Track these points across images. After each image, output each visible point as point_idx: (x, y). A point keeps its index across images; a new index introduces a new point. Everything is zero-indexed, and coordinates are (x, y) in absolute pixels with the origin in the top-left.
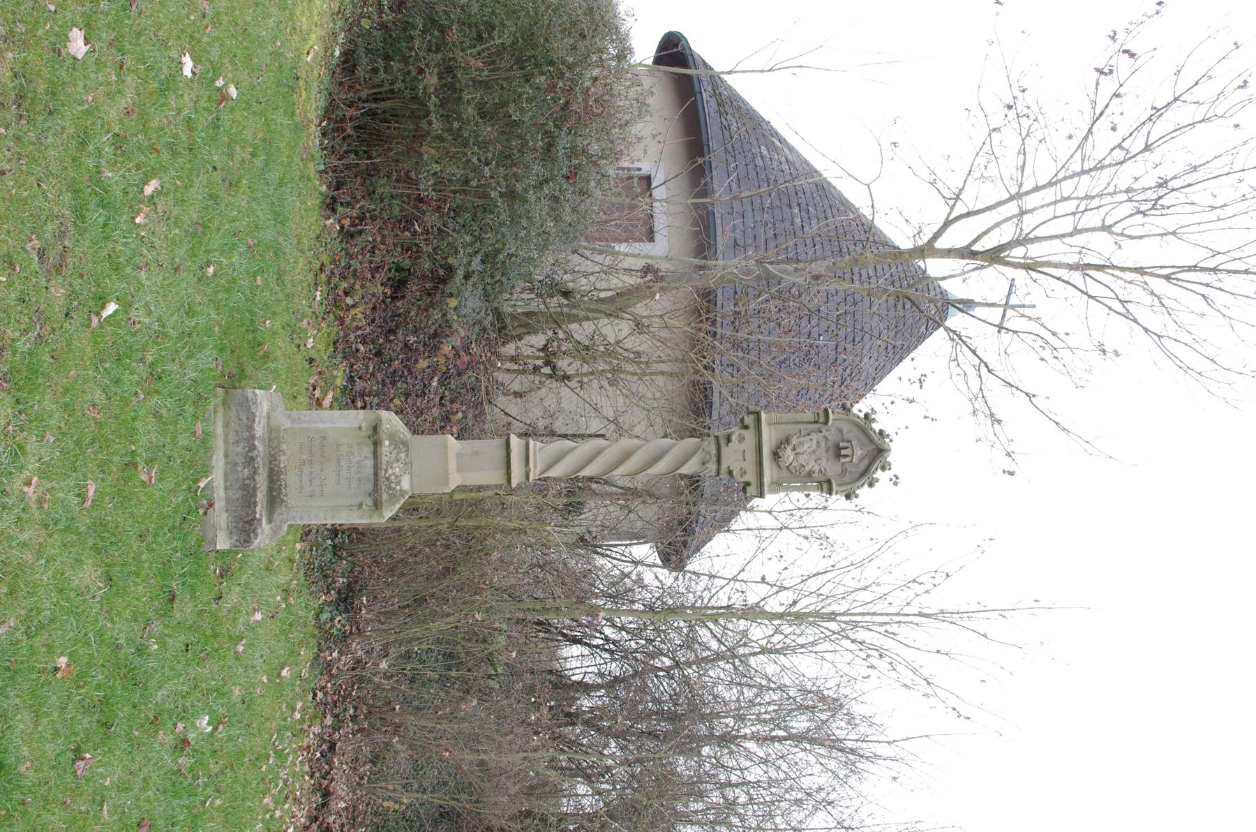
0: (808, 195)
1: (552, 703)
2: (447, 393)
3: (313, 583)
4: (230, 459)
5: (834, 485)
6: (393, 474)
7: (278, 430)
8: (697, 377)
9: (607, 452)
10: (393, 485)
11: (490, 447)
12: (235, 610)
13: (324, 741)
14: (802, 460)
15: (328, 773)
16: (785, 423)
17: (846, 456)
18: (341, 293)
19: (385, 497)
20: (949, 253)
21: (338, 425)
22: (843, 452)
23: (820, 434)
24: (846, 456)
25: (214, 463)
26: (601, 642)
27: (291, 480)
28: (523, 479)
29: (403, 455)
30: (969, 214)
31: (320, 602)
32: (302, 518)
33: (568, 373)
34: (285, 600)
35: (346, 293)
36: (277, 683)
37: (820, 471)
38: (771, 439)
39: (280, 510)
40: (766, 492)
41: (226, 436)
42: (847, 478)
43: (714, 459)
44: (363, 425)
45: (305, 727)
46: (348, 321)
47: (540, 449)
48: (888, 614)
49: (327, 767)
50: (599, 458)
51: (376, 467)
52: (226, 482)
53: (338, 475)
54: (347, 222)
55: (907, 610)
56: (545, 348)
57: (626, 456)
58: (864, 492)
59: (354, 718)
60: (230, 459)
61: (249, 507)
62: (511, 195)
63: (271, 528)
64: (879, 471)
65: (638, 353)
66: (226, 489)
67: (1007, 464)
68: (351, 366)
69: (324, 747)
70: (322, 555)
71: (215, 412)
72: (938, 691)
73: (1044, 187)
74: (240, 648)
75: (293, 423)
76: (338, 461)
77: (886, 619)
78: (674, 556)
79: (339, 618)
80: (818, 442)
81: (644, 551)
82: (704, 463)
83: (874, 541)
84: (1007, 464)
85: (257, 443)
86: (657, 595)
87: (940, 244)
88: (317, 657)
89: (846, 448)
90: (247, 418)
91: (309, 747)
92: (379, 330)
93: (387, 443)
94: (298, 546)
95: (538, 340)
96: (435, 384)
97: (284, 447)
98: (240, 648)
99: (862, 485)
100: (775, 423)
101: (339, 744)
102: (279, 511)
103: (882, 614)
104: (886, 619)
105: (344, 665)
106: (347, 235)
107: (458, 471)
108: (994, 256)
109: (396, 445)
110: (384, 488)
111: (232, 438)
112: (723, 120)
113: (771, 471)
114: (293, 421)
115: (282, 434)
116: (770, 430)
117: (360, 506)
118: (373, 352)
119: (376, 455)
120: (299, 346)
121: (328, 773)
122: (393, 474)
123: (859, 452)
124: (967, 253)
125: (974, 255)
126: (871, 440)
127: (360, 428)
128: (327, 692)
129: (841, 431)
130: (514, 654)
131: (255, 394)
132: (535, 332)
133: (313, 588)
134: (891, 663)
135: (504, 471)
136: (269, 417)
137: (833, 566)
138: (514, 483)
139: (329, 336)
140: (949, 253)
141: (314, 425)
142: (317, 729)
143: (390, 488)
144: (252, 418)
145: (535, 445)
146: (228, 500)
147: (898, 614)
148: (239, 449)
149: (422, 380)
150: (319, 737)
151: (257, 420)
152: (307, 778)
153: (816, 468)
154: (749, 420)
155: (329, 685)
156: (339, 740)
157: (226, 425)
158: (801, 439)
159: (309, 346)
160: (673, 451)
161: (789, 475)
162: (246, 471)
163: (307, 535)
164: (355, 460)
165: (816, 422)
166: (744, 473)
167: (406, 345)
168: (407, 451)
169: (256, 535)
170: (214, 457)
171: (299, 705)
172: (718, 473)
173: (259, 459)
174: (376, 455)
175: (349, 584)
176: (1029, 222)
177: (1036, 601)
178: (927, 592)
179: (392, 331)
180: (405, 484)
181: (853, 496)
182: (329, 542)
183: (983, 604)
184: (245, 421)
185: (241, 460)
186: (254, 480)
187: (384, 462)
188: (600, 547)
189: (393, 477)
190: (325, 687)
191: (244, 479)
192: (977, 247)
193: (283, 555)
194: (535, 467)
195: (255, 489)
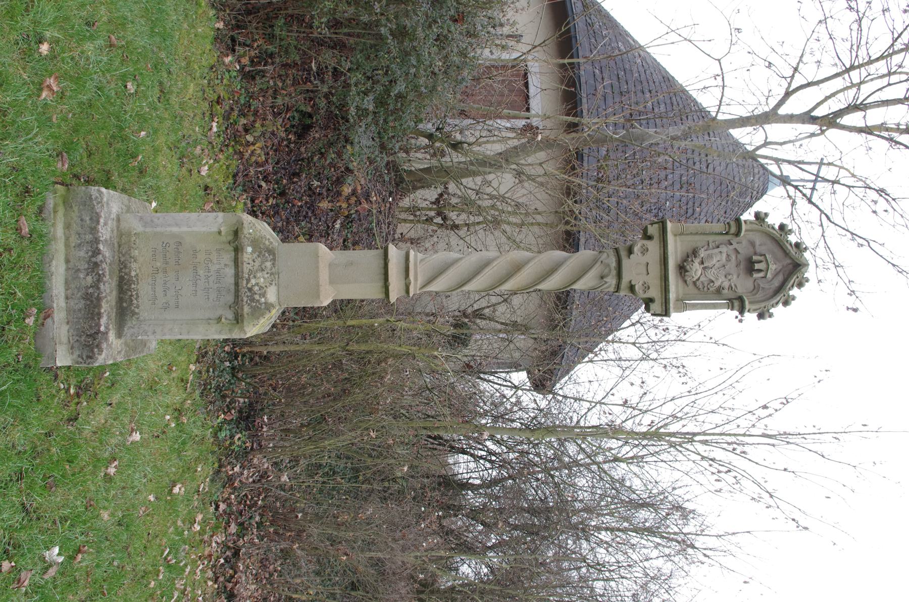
0: (657, 84)
1: (440, 513)
2: (349, 236)
4: (71, 265)
5: (747, 303)
6: (257, 284)
7: (129, 234)
8: (568, 228)
9: (495, 263)
10: (257, 297)
11: (366, 258)
12: (102, 431)
13: (229, 548)
14: (711, 275)
15: (232, 577)
16: (691, 234)
17: (760, 271)
18: (240, 129)
19: (246, 309)
20: (790, 118)
21: (195, 229)
22: (757, 266)
23: (731, 247)
24: (760, 271)
25: (53, 269)
26: (484, 453)
27: (143, 290)
28: (403, 293)
29: (268, 264)
30: (809, 84)
31: (219, 421)
33: (456, 223)
34: (177, 419)
35: (247, 131)
36: (169, 502)
37: (730, 287)
38: (676, 252)
39: (131, 323)
40: (671, 310)
41: (67, 239)
42: (760, 296)
43: (614, 272)
44: (222, 229)
45: (206, 537)
46: (247, 155)
47: (422, 260)
48: (735, 435)
49: (231, 572)
50: (486, 270)
51: (237, 276)
52: (67, 290)
54: (245, 61)
55: (753, 431)
56: (437, 201)
57: (517, 268)
58: (778, 311)
59: (260, 525)
60: (71, 265)
61: (93, 319)
62: (401, 33)
64: (795, 288)
65: (518, 205)
66: (67, 298)
67: (851, 302)
68: (253, 201)
69: (228, 553)
71: (55, 212)
72: (779, 503)
73: (877, 60)
74: (112, 471)
75: (145, 226)
77: (733, 439)
78: (541, 385)
79: (239, 435)
80: (728, 255)
81: (520, 377)
82: (602, 278)
83: (723, 370)
84: (851, 302)
85: (101, 247)
86: (532, 415)
87: (783, 111)
88: (218, 472)
89: (760, 262)
90: (91, 219)
91: (210, 556)
92: (283, 172)
93: (249, 249)
94: (192, 367)
95: (431, 194)
96: (337, 226)
97: (136, 253)
98: (112, 471)
99: (777, 303)
100: (682, 234)
101: (243, 550)
102: (129, 324)
103: (730, 435)
104: (733, 439)
105: (247, 478)
106: (249, 76)
107: (332, 282)
108: (830, 121)
109: (260, 253)
110: (245, 299)
111: (74, 240)
112: (587, 18)
113: (677, 286)
114: (145, 225)
115: (133, 239)
116: (675, 241)
117: (219, 319)
118: (278, 191)
119: (237, 262)
121: (232, 577)
122: (257, 284)
123: (773, 267)
124: (808, 118)
125: (814, 120)
126: (786, 253)
127: (220, 233)
128: (231, 503)
129: (752, 244)
130: (406, 469)
131: (100, 193)
132: (429, 186)
134: (735, 477)
135: (381, 284)
136: (118, 220)
137: (689, 392)
138: (393, 298)
139: (228, 168)
140: (790, 118)
141: (168, 229)
142: (220, 538)
143: (253, 300)
144: (96, 219)
145: (416, 256)
146: (69, 311)
147: (744, 435)
148: (82, 254)
149: (326, 222)
150: (225, 546)
151: (102, 221)
152: (210, 583)
153: (726, 284)
154: (653, 230)
155: (233, 496)
156: (243, 546)
157: (67, 226)
158: (709, 252)
159: (203, 173)
160: (568, 263)
161: (696, 291)
162: (89, 279)
163: (203, 357)
164: (214, 268)
165: (727, 233)
166: (647, 288)
167: (310, 189)
168: (274, 259)
169: (101, 351)
170: (54, 263)
171: (199, 517)
172: (618, 288)
173: (104, 265)
174: (237, 262)
175: (251, 404)
176: (866, 89)
177: (865, 425)
178: (770, 415)
179: (296, 174)
180: (272, 295)
181: (767, 315)
182: (227, 364)
183: (817, 427)
184: (88, 222)
185: (83, 266)
186: (98, 288)
187: (246, 271)
188: (485, 373)
189: (256, 288)
190: (229, 499)
191: (87, 288)
192: (816, 113)
194: (416, 279)
195: (99, 299)
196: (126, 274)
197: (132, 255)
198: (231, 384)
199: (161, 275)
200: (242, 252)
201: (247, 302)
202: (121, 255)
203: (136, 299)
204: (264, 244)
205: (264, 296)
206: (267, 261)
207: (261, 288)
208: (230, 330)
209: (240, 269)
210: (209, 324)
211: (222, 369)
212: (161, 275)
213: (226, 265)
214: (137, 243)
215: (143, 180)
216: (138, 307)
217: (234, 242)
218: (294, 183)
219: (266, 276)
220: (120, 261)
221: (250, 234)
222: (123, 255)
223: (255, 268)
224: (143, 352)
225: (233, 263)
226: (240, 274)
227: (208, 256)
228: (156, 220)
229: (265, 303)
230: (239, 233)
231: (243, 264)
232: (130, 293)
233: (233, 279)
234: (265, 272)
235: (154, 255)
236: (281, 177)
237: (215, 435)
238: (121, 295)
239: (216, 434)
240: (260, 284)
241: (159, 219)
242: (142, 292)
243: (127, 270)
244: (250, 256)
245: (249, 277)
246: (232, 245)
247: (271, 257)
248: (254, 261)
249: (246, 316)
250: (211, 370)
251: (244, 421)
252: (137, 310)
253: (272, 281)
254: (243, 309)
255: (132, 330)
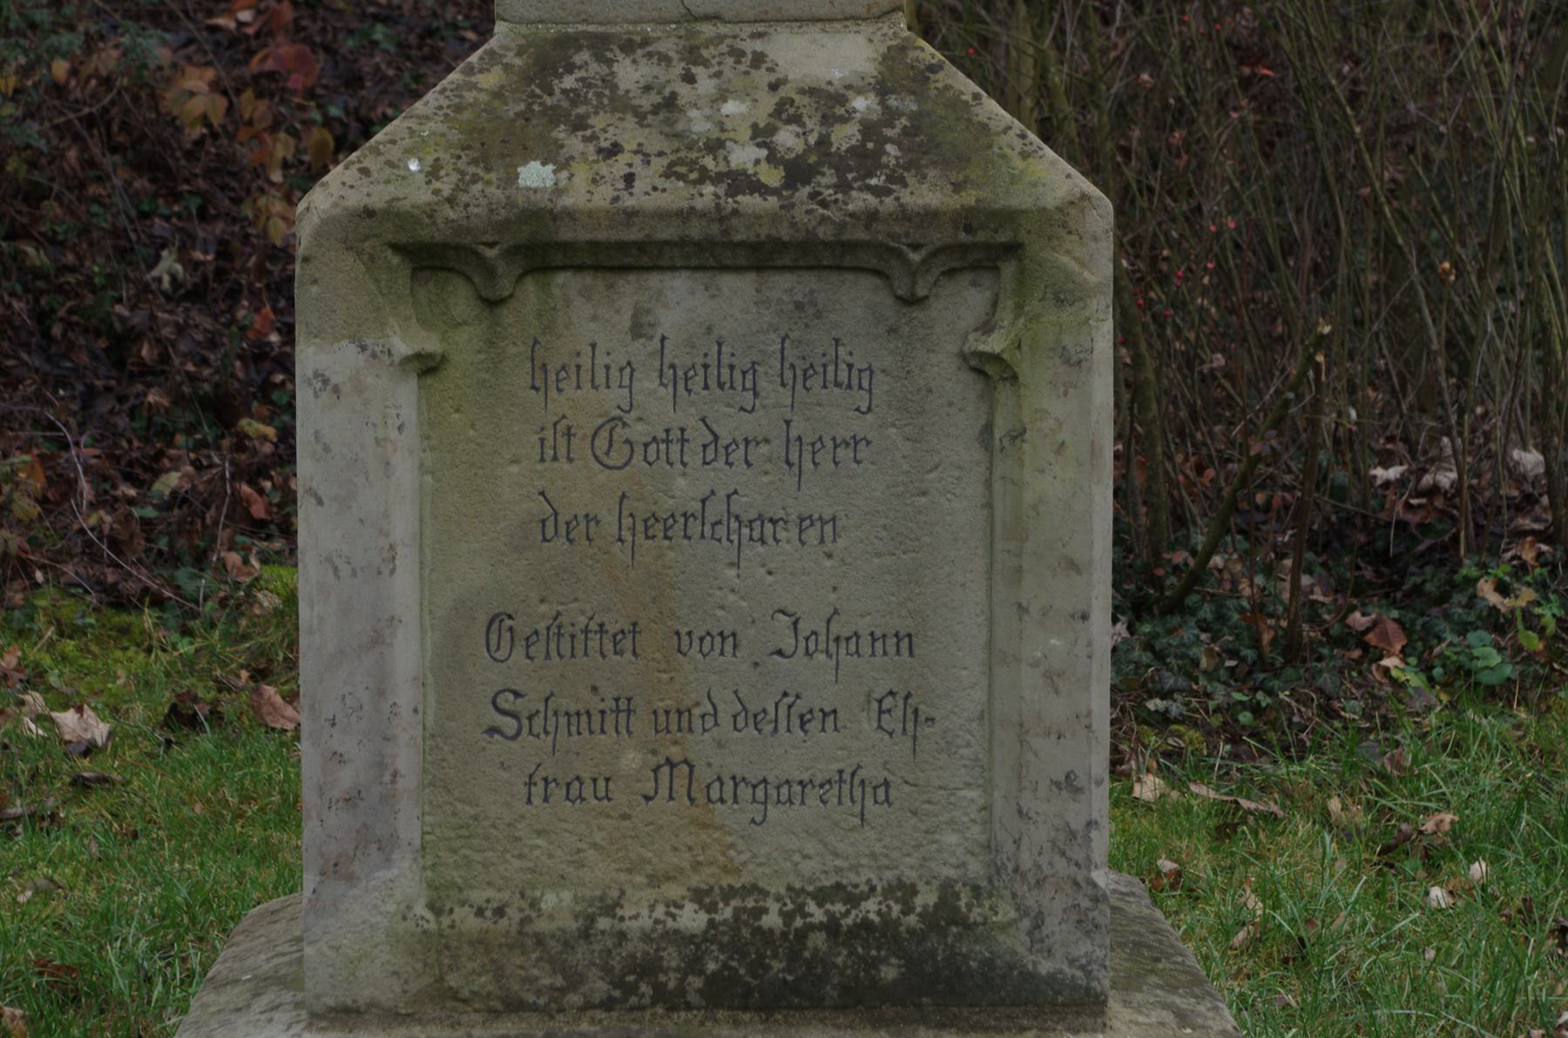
3: (1330, 713)
6: (762, 135)
10: (845, 136)
19: (925, 194)
21: (403, 526)
29: (630, 74)
31: (1415, 680)
32: (1070, 784)
34: (1433, 861)
44: (402, 348)
53: (765, 524)
63: (1129, 983)
70: (1190, 668)
75: (386, 847)
76: (657, 525)
93: (535, 175)
97: (558, 906)
102: (1015, 943)
109: (555, 116)
110: (860, 200)
118: (207, 432)
120: (81, 785)
127: (427, 367)
133: (1352, 709)
139: (77, 632)
141: (404, 695)
143: (864, 159)
159: (99, 730)
168: (600, 45)
187: (676, 195)
189: (788, 139)
193: (1203, 866)
196: (693, 965)
197: (573, 925)
198: (1221, 617)
199: (700, 746)
200: (554, 216)
201: (878, 192)
202: (575, 999)
203: (854, 900)
204: (497, 94)
205: (841, 99)
206: (609, 82)
207: (785, 113)
208: (1066, 294)
209: (667, 233)
210: (1018, 435)
211: (1146, 657)
212: (700, 746)
213: (638, 330)
214: (498, 897)
215: (120, 983)
216: (904, 892)
217: (490, 272)
218: (164, 358)
219: (706, 84)
220: (608, 1004)
221: (433, 172)
222: (575, 981)
223: (655, 143)
224: (1149, 921)
225: (628, 286)
226: (695, 231)
227: (580, 446)
228: (346, 778)
229: (882, 89)
230: (425, 234)
231: (631, 215)
232: (818, 940)
233: (729, 282)
234: (684, 90)
235: (573, 788)
236: (132, 414)
237: (1495, 695)
238: (831, 992)
239: (1492, 693)
240: (762, 118)
241: (338, 758)
242: (808, 867)
243: (672, 957)
244: (582, 175)
245: (717, 179)
246: (504, 286)
247: (583, 56)
248: (615, 150)
249: (969, 198)
250: (1154, 704)
251: (1403, 574)
252: (927, 898)
253: (738, 54)
254: (930, 217)
255: (1051, 924)
